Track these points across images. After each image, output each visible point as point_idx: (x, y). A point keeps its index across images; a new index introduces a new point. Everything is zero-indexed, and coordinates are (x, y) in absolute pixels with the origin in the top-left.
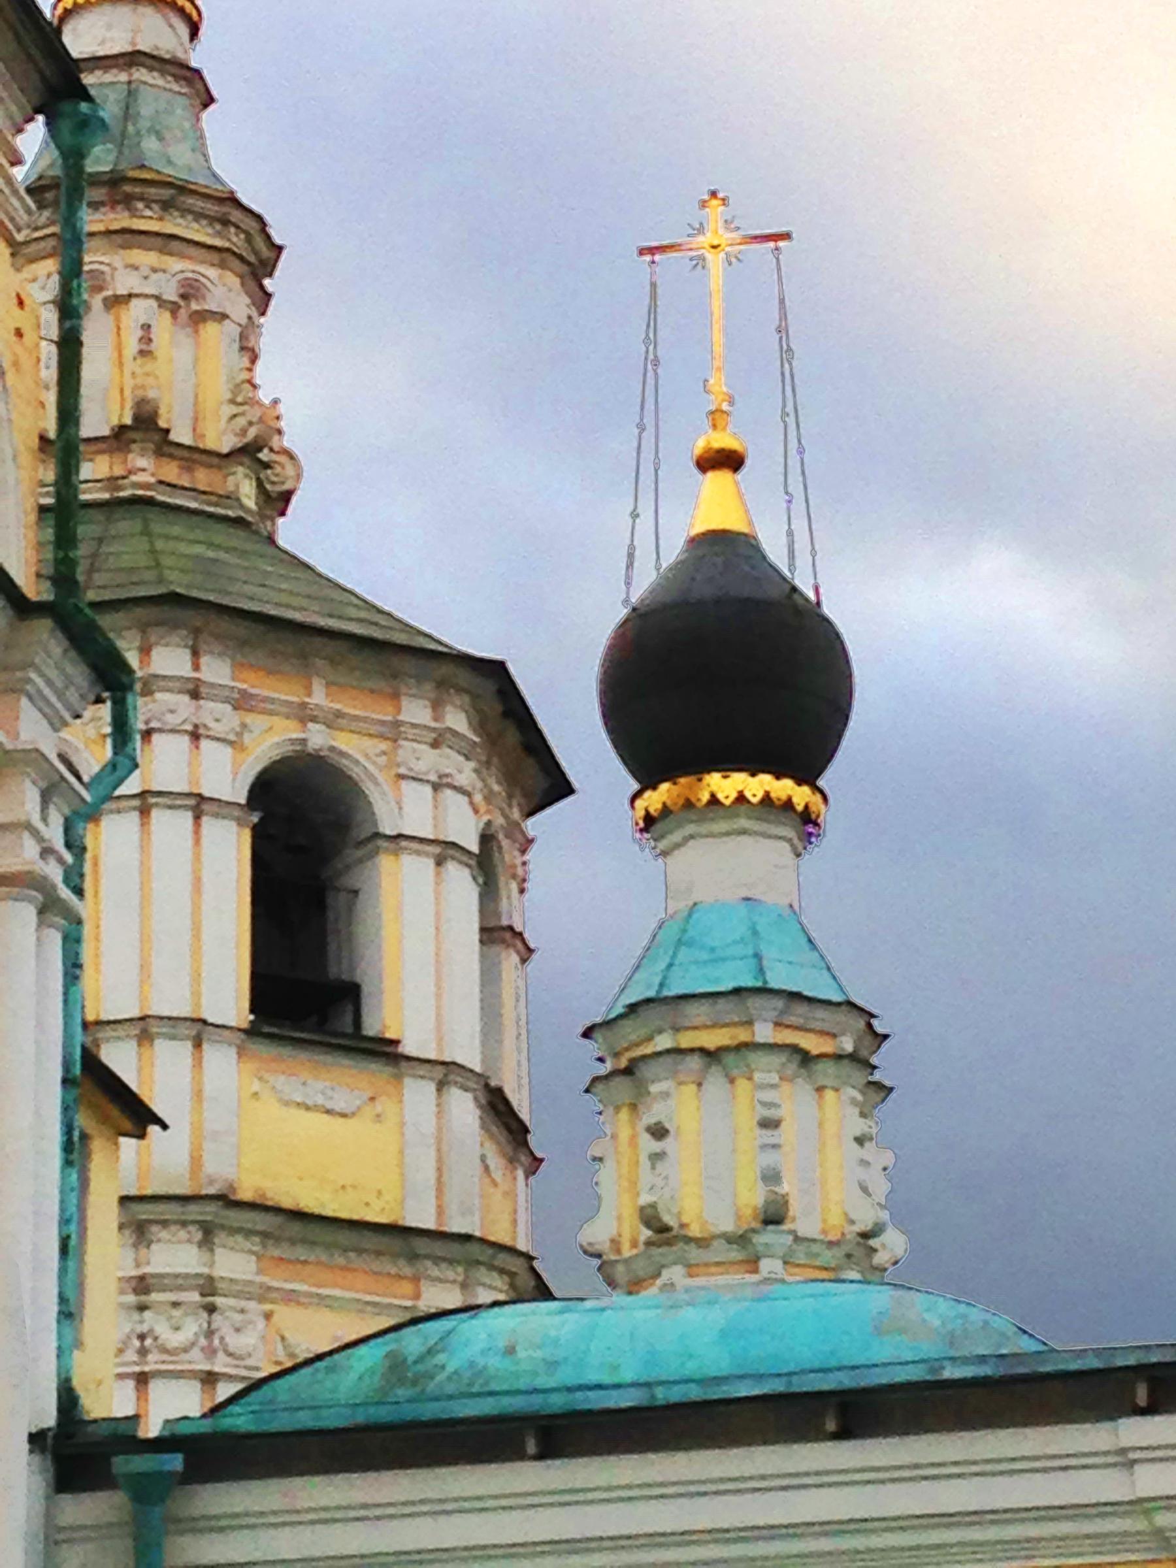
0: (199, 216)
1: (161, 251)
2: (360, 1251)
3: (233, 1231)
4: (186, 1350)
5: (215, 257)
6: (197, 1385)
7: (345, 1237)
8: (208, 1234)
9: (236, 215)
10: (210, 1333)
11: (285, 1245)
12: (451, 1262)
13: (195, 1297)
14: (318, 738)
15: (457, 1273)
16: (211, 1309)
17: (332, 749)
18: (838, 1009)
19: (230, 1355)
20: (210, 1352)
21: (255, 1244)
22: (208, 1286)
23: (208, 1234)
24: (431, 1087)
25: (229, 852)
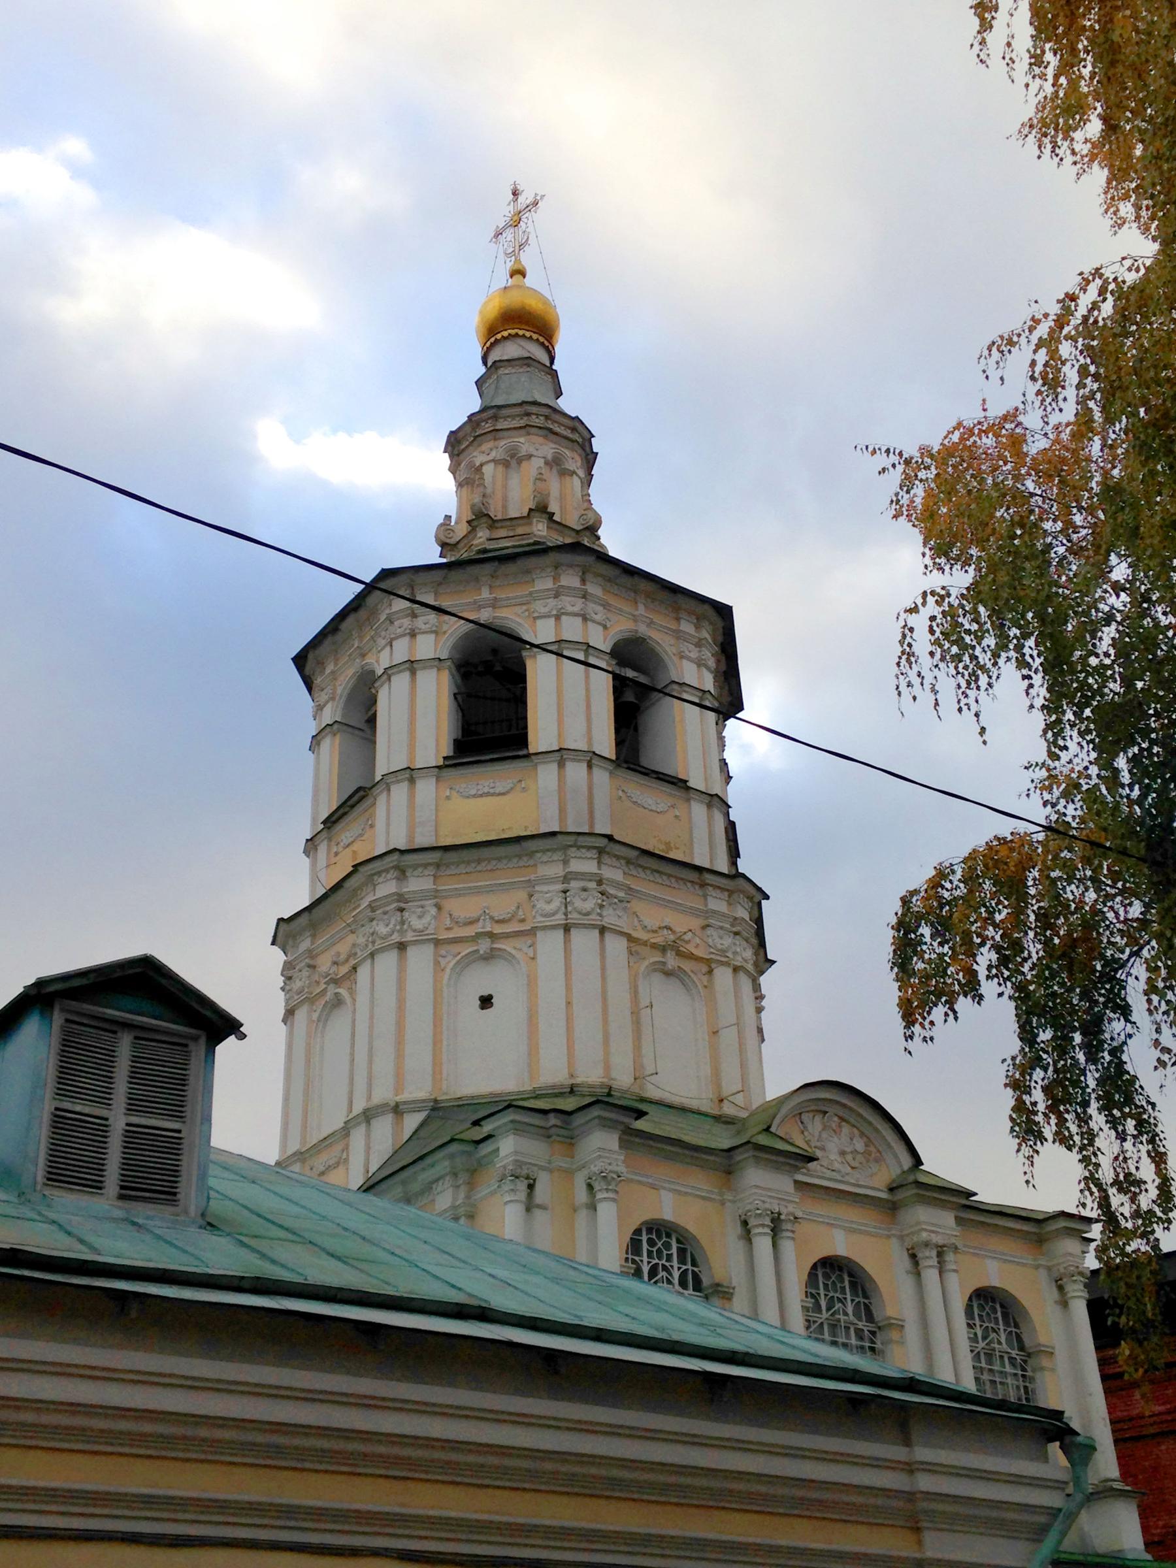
0: (513, 417)
1: (495, 439)
2: (499, 859)
3: (415, 867)
4: (554, 914)
5: (523, 432)
6: (396, 951)
7: (474, 854)
8: (402, 873)
9: (580, 428)
10: (403, 923)
11: (525, 859)
12: (553, 850)
13: (593, 885)
14: (643, 630)
15: (558, 856)
16: (402, 910)
17: (494, 618)
18: (339, 637)
19: (415, 931)
20: (402, 932)
21: (431, 871)
22: (400, 897)
23: (402, 873)
24: (555, 766)
25: (603, 684)
